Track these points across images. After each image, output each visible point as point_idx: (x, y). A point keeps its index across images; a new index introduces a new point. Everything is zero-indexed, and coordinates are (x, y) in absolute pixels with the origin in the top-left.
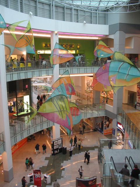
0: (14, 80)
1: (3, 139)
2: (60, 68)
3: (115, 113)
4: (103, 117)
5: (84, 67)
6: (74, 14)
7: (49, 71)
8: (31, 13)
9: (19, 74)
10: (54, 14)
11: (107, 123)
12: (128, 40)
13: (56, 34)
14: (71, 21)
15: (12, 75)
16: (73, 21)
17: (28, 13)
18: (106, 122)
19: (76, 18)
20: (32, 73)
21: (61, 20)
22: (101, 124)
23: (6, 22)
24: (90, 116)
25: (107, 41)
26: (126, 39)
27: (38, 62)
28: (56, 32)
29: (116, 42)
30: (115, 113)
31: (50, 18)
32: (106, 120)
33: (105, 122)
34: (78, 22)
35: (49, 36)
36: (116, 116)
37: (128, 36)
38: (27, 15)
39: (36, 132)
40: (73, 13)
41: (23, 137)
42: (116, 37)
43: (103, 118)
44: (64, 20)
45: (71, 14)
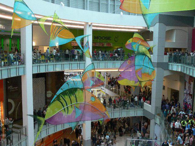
0: (41, 72)
1: (26, 134)
2: (34, 65)
3: (153, 113)
4: (142, 116)
5: (60, 63)
6: (110, 4)
7: (41, 67)
8: (62, 3)
9: (47, 66)
10: (88, 5)
11: (146, 124)
12: (169, 34)
13: (90, 26)
14: (107, 12)
15: (39, 67)
16: (109, 12)
17: (59, 4)
18: (144, 123)
19: (98, 8)
20: (53, 66)
21: (81, 9)
22: (139, 124)
23: (34, 13)
24: (119, 116)
25: (146, 35)
26: (166, 31)
27: (68, 53)
28: (90, 23)
29: (156, 36)
30: (153, 113)
31: (84, 9)
32: (144, 121)
33: (143, 123)
34: (114, 13)
35: (82, 27)
36: (154, 117)
37: (169, 28)
38: (58, 6)
39: (56, 132)
40: (109, 4)
41: (49, 134)
42: (155, 29)
43: (141, 119)
44: (99, 11)
45: (107, 5)
